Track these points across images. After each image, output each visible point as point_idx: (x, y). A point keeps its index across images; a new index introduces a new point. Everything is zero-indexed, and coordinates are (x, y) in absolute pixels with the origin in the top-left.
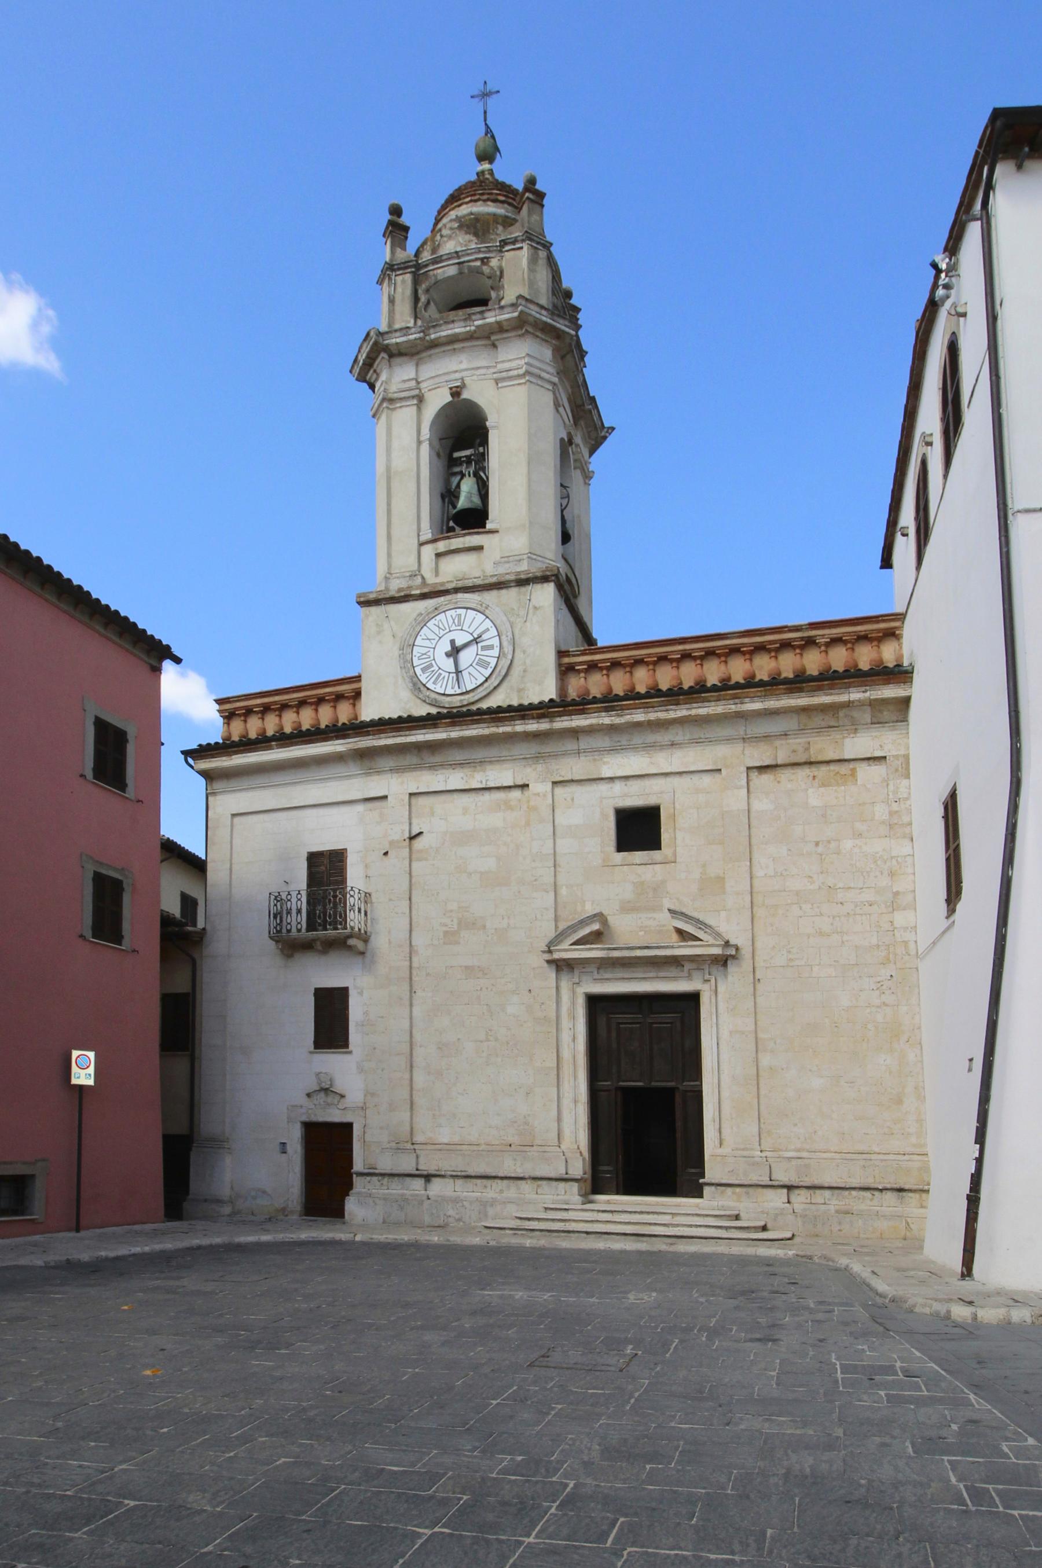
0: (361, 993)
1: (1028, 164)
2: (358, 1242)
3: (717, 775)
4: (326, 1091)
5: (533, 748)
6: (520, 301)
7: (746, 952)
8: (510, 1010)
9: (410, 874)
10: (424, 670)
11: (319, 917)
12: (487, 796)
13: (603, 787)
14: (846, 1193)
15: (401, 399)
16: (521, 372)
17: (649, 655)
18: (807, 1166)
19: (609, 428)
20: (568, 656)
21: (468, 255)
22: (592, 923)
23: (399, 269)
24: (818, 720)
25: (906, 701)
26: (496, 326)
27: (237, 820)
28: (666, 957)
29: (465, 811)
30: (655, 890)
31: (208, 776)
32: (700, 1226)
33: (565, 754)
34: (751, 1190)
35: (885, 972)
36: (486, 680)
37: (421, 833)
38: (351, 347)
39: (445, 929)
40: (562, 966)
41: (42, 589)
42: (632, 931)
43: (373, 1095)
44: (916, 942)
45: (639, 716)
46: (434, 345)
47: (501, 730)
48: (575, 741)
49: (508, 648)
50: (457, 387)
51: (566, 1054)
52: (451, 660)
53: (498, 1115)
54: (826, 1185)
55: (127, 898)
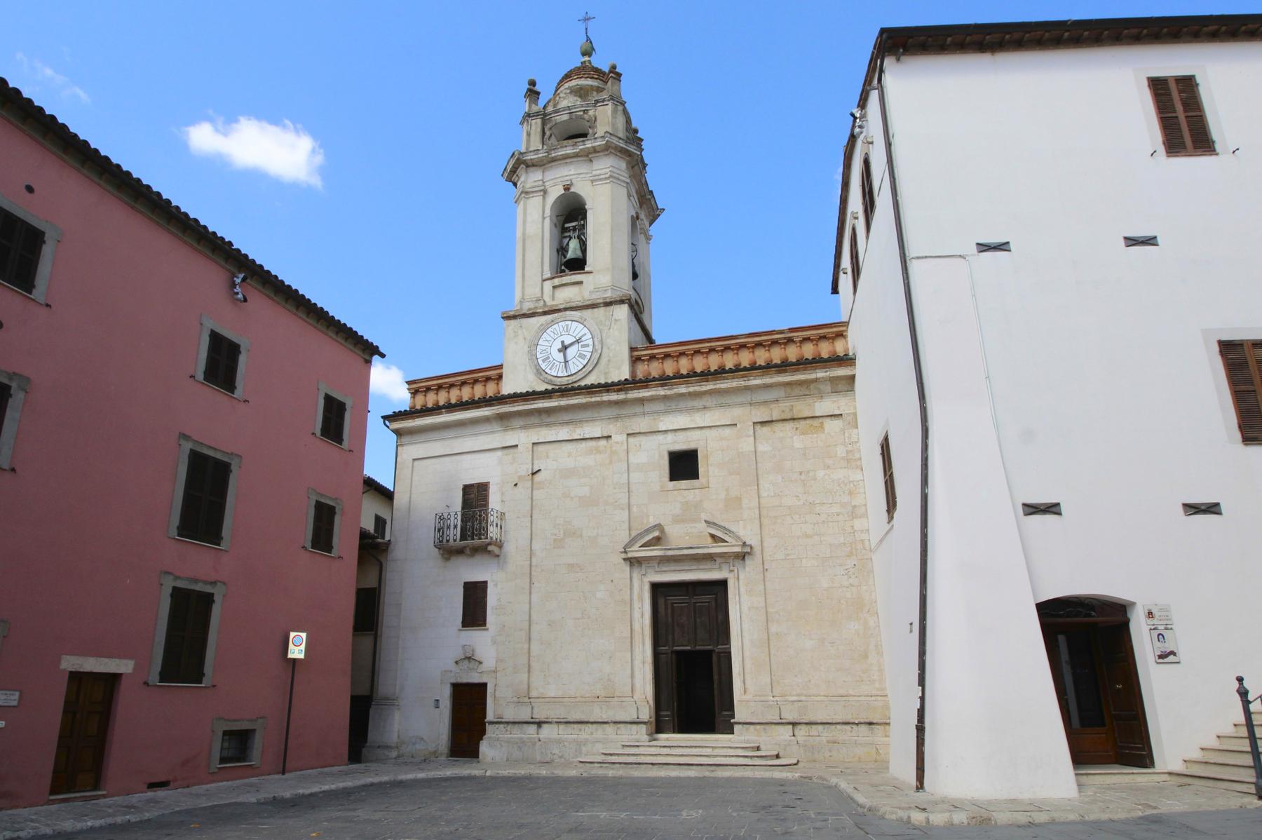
0: (496, 585)
5: (614, 411)
7: (757, 549)
8: (599, 595)
12: (584, 445)
13: (660, 437)
24: (797, 391)
25: (853, 377)
27: (416, 463)
29: (570, 455)
31: (398, 433)
33: (635, 415)
34: (767, 727)
38: (503, 161)
40: (634, 562)
42: (683, 536)
46: (554, 160)
47: (593, 399)
49: (598, 347)
51: (637, 626)
55: (337, 519)
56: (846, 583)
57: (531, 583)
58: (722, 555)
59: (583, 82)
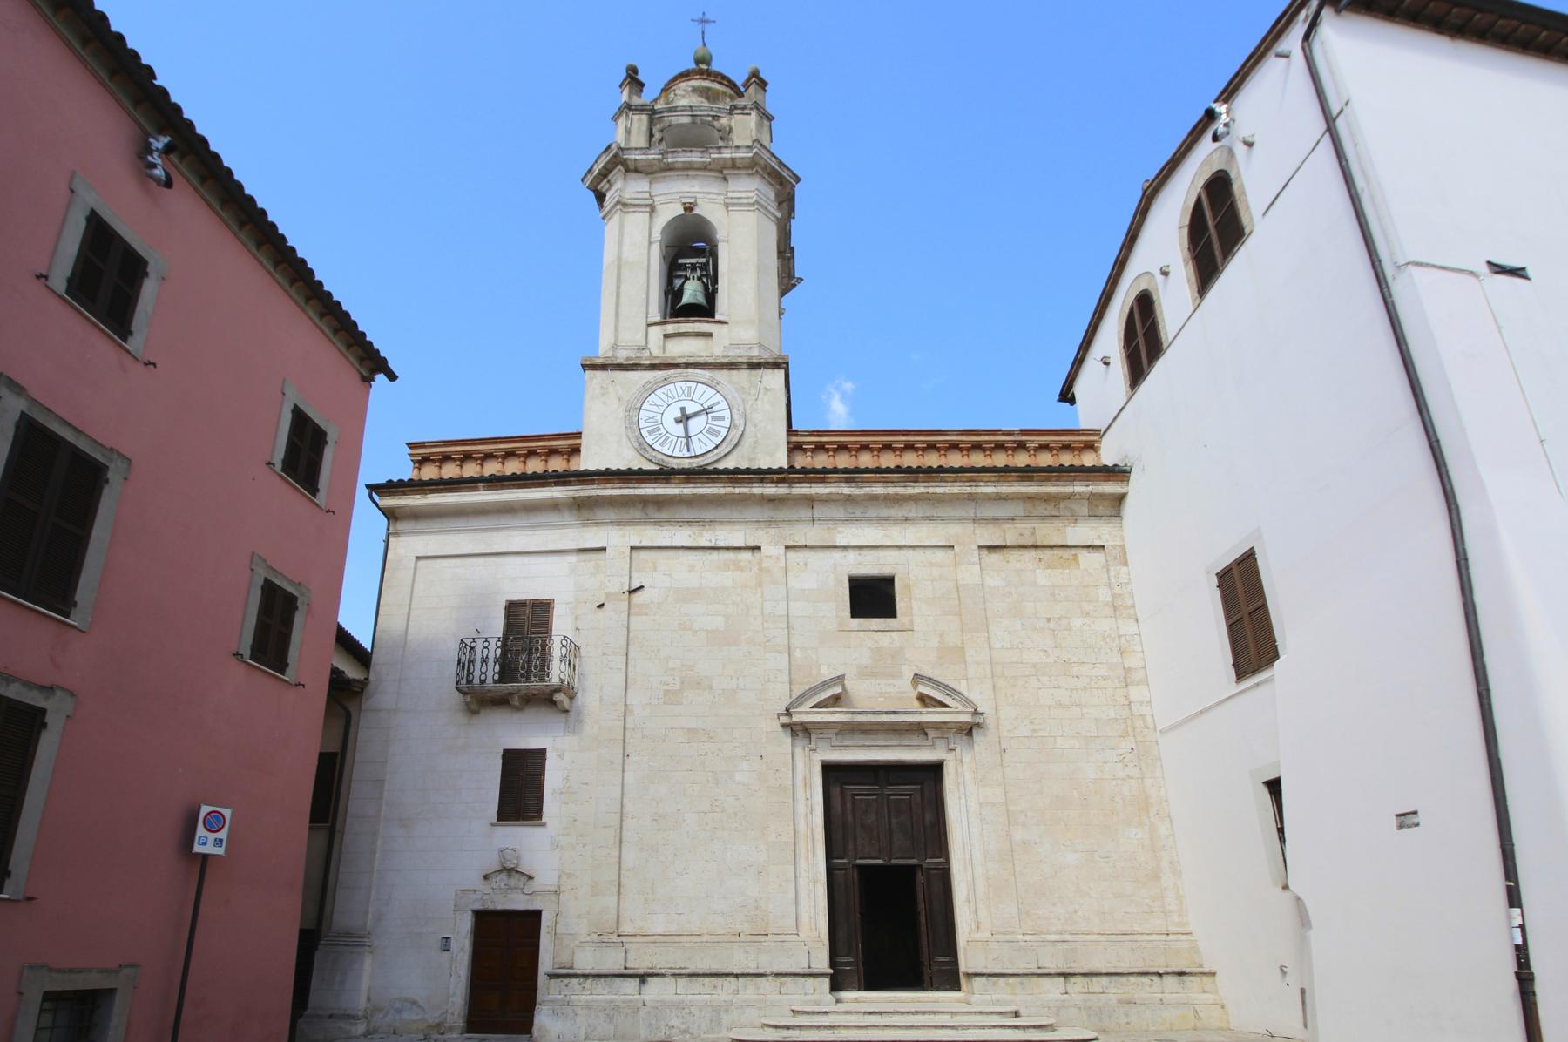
0: (561, 756)
1: (1344, 13)
3: (949, 551)
4: (510, 871)
5: (767, 512)
7: (990, 721)
8: (739, 777)
10: (650, 432)
12: (715, 555)
14: (1124, 979)
24: (1042, 509)
25: (1120, 499)
27: (421, 563)
28: (911, 724)
29: (692, 569)
31: (391, 515)
33: (799, 520)
34: (1025, 980)
35: (1126, 745)
38: (589, 156)
40: (800, 731)
41: (258, 248)
43: (569, 875)
47: (737, 490)
49: (739, 421)
51: (802, 827)
52: (681, 426)
55: (299, 619)
57: (625, 756)
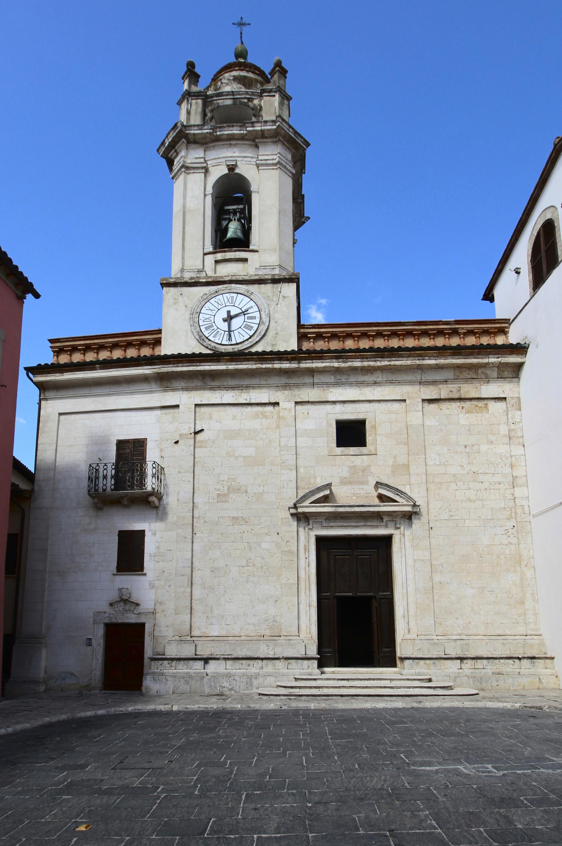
0: (154, 534)
2: (175, 711)
3: (403, 404)
5: (283, 380)
6: (278, 119)
7: (423, 510)
8: (264, 546)
9: (194, 456)
11: (129, 482)
12: (249, 409)
13: (329, 407)
15: (194, 168)
16: (275, 162)
17: (356, 332)
18: (467, 644)
19: (307, 217)
20: (304, 328)
21: (240, 94)
22: (325, 490)
23: (194, 96)
26: (260, 133)
27: (62, 417)
29: (234, 418)
30: (363, 471)
32: (416, 687)
33: (304, 385)
34: (436, 661)
36: (250, 338)
37: (202, 430)
38: (161, 133)
39: (219, 492)
40: (302, 518)
42: (348, 496)
43: (161, 603)
44: (529, 506)
45: (357, 363)
46: (218, 139)
47: (264, 366)
48: (312, 378)
49: (265, 319)
50: (233, 165)
51: (302, 574)
53: (255, 615)
54: (485, 656)
56: (505, 542)
57: (193, 533)
58: (389, 514)
59: (243, 73)
